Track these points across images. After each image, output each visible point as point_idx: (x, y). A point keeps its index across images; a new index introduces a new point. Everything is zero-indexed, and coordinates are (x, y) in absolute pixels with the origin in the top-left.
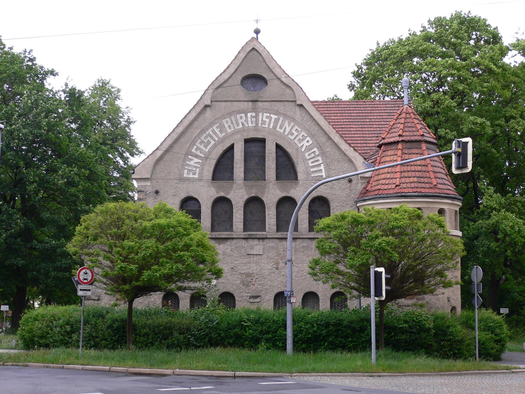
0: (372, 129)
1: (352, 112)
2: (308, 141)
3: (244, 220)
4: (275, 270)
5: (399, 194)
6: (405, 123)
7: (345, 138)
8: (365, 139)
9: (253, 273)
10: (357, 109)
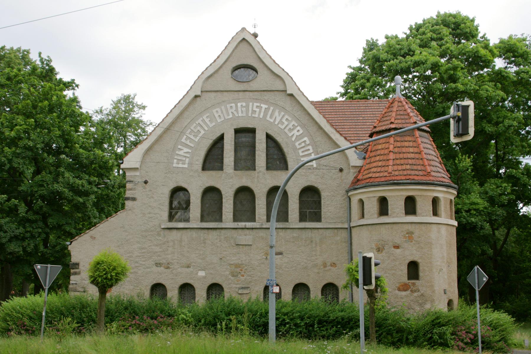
0: (365, 127)
1: (346, 111)
2: (298, 131)
3: (234, 211)
4: (265, 261)
5: (391, 182)
6: (397, 111)
7: (335, 127)
8: (358, 135)
9: (242, 264)
10: (351, 108)
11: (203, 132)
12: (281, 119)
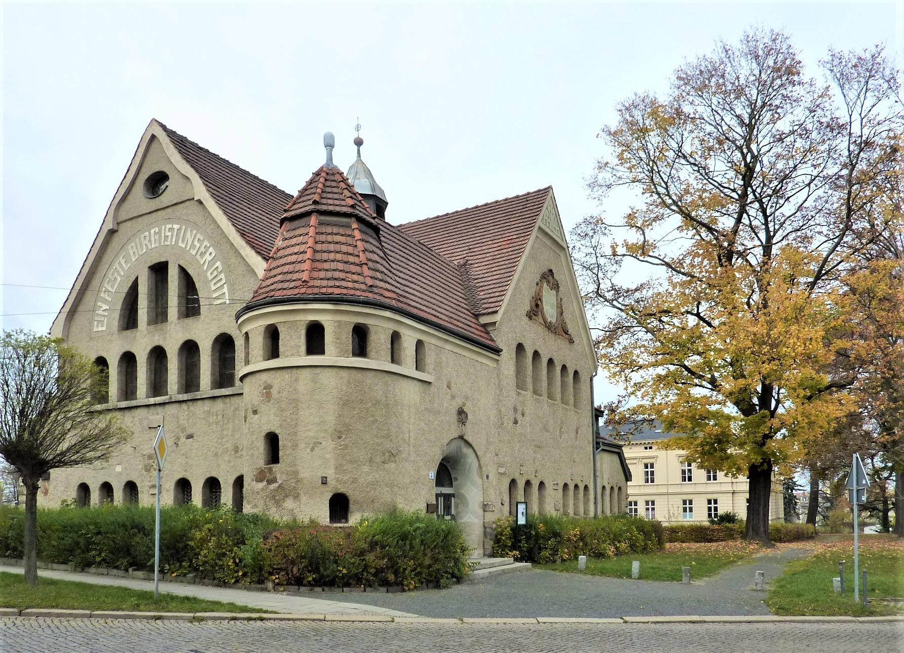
11: (119, 279)
12: (193, 241)
